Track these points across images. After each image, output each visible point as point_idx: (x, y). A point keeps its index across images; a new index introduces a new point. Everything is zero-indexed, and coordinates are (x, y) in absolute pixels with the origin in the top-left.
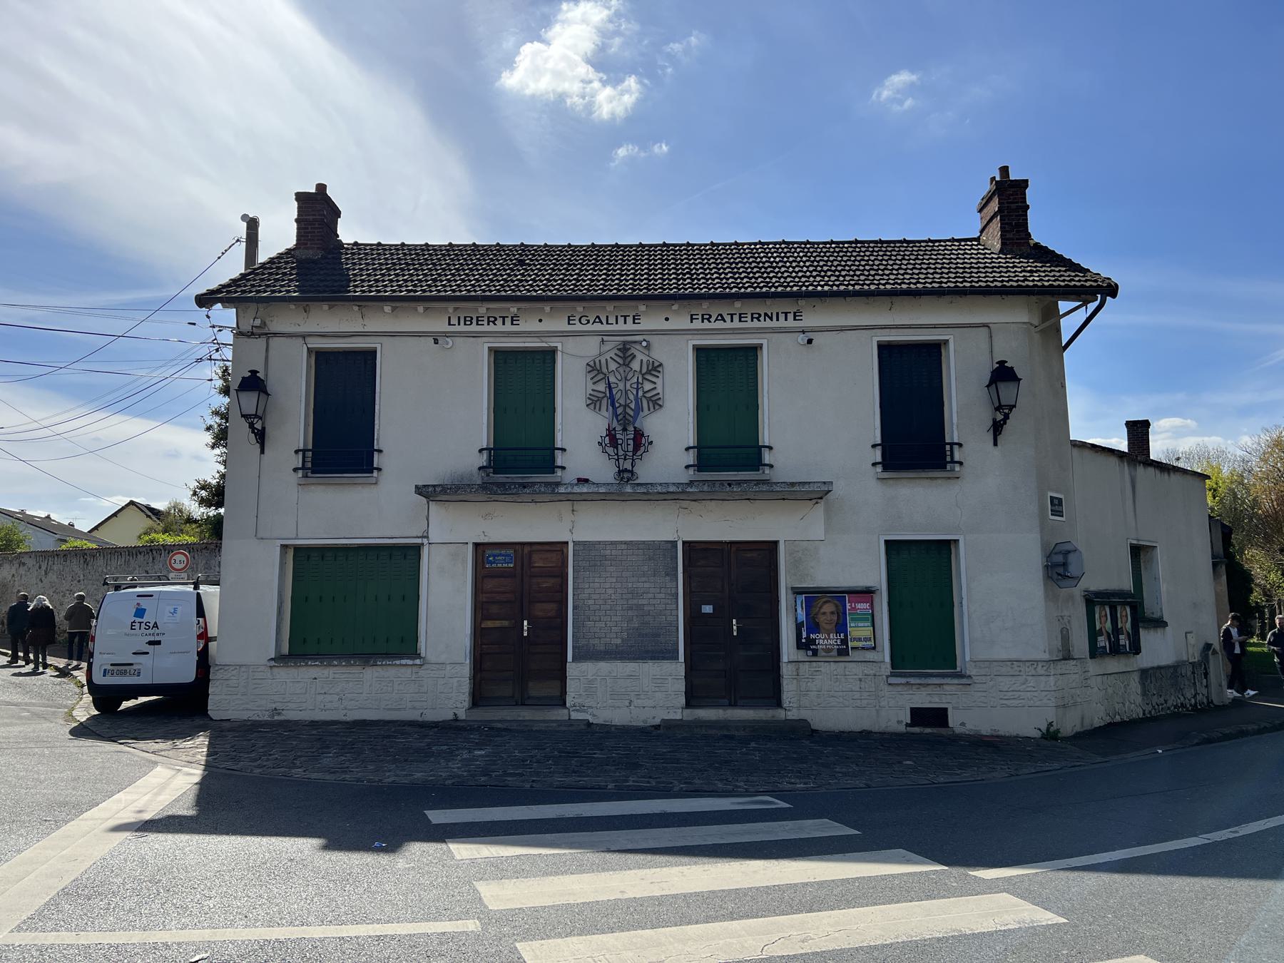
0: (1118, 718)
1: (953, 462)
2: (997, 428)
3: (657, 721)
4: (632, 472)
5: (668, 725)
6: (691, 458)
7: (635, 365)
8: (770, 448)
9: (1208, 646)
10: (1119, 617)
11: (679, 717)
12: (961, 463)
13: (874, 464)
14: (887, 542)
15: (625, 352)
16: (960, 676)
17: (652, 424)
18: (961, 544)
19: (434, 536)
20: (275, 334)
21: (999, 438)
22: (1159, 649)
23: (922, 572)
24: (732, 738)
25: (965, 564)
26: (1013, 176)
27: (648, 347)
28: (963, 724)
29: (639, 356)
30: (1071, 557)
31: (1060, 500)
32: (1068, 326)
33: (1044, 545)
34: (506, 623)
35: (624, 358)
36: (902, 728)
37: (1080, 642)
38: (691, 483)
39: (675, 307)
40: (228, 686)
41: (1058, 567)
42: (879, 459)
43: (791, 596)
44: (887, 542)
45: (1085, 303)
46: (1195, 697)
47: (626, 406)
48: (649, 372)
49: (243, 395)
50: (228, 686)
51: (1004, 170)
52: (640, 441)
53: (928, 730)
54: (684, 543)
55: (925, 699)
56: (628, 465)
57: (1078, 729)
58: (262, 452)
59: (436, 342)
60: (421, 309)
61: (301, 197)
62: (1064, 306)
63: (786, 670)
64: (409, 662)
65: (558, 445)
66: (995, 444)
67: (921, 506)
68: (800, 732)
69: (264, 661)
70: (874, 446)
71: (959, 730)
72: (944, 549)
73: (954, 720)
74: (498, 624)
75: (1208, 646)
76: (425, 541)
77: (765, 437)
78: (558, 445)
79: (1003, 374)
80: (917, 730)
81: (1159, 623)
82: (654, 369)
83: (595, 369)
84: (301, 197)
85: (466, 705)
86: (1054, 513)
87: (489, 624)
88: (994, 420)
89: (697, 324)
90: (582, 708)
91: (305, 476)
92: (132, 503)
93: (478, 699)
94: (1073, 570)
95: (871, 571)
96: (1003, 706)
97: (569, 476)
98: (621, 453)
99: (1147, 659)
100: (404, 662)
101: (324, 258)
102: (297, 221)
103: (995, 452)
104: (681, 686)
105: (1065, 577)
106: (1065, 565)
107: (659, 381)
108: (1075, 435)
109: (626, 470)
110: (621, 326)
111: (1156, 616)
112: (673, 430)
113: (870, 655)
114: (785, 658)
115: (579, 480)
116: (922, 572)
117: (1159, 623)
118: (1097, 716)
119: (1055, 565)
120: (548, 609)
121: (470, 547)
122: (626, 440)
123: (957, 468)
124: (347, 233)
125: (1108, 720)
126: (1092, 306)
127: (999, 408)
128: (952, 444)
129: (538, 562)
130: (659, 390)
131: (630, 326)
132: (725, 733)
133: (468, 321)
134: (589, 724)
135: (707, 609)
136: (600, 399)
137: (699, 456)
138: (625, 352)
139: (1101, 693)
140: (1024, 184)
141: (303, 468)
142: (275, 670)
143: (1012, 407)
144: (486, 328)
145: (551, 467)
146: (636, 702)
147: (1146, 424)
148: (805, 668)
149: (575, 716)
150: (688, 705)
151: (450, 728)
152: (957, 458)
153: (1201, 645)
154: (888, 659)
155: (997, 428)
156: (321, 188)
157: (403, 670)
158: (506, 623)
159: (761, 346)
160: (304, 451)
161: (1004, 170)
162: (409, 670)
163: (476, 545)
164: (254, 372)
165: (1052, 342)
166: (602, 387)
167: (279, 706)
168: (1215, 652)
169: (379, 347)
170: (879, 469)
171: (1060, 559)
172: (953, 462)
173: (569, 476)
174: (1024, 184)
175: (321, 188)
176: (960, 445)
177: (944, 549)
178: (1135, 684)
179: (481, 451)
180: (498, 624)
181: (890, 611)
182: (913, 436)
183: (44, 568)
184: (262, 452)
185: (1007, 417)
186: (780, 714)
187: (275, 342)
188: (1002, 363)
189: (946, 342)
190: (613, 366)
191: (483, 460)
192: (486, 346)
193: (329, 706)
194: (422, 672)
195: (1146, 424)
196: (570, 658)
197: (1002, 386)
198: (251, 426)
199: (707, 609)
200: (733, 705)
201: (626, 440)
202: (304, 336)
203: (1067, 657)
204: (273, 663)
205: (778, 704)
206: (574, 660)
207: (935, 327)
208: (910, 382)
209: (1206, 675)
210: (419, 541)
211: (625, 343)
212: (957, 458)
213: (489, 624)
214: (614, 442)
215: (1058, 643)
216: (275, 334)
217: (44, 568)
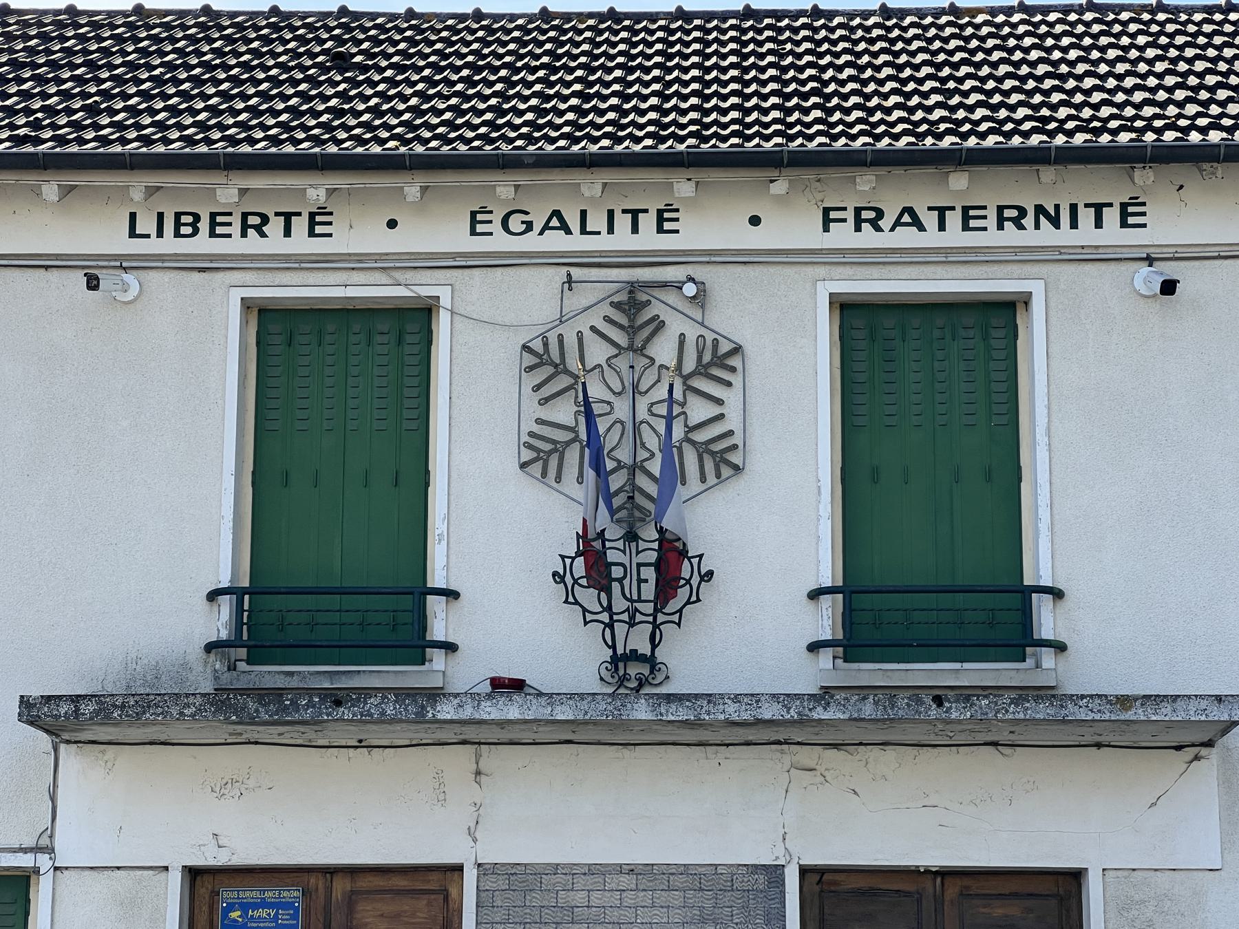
6: (824, 621)
7: (664, 350)
15: (634, 313)
17: (710, 520)
27: (699, 299)
29: (676, 325)
35: (631, 330)
38: (826, 695)
39: (779, 187)
48: (702, 370)
52: (674, 568)
54: (804, 871)
59: (93, 283)
65: (437, 578)
76: (44, 862)
77: (1040, 565)
78: (437, 578)
82: (720, 360)
83: (546, 362)
97: (466, 672)
98: (619, 604)
107: (731, 398)
109: (634, 656)
110: (623, 240)
112: (773, 542)
115: (497, 683)
121: (175, 882)
122: (637, 568)
130: (733, 421)
131: (649, 239)
136: (559, 449)
137: (849, 617)
138: (634, 313)
163: (194, 874)
166: (565, 411)
173: (466, 672)
179: (213, 596)
190: (598, 352)
192: (236, 295)
201: (637, 568)
210: (26, 861)
211: (633, 287)
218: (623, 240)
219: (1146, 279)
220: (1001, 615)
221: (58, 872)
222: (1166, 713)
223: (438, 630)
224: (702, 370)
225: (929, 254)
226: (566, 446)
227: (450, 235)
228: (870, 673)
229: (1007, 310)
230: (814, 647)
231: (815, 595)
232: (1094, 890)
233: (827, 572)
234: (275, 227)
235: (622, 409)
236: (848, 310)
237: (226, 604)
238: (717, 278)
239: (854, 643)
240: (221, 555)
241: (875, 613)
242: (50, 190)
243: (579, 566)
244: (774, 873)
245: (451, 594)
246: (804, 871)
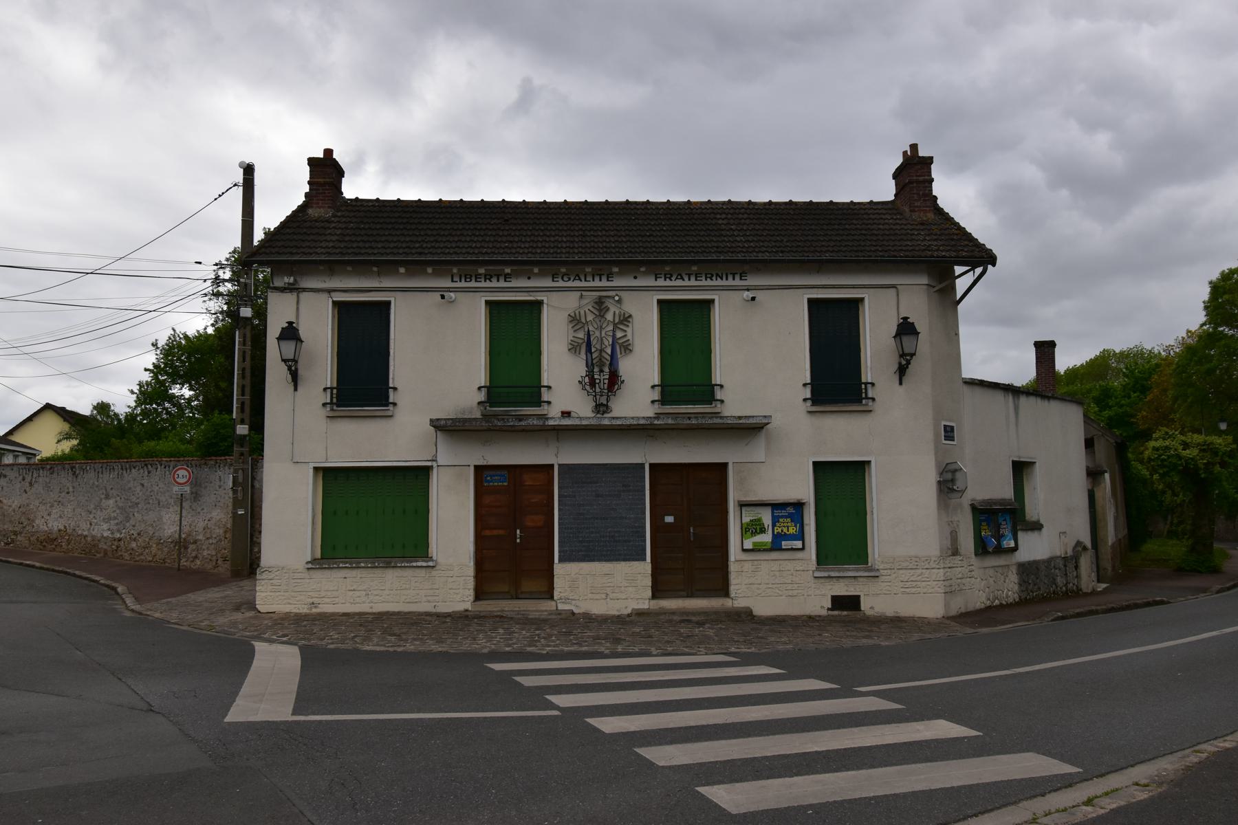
0: (997, 602)
1: (867, 398)
2: (902, 371)
3: (629, 611)
4: (607, 406)
5: (640, 613)
6: (656, 395)
7: (609, 316)
8: (722, 386)
9: (1079, 543)
10: (998, 522)
11: (646, 607)
12: (873, 399)
13: (805, 400)
14: (815, 463)
15: (600, 306)
16: (871, 569)
17: (626, 366)
18: (873, 464)
19: (441, 461)
20: (304, 290)
21: (904, 379)
22: (1032, 549)
23: (842, 481)
24: (689, 621)
25: (875, 480)
26: (922, 153)
27: (619, 301)
28: (872, 608)
29: (613, 309)
30: (958, 475)
31: (952, 428)
32: (961, 284)
33: (938, 464)
34: (501, 532)
35: (600, 310)
36: (824, 613)
37: (967, 542)
38: (658, 416)
39: (643, 269)
40: (272, 585)
41: (948, 484)
42: (809, 396)
43: (738, 509)
44: (815, 463)
45: (973, 269)
46: (1066, 585)
47: (601, 351)
48: (621, 322)
49: (283, 343)
50: (272, 585)
51: (914, 147)
52: (614, 380)
53: (845, 613)
54: (651, 465)
55: (842, 589)
56: (603, 400)
57: (963, 610)
58: (296, 389)
59: (443, 297)
60: (430, 270)
61: (312, 162)
62: (958, 270)
63: (733, 567)
64: (424, 564)
65: (545, 383)
66: (901, 383)
67: (841, 437)
68: (745, 616)
69: (301, 565)
70: (805, 385)
71: (869, 613)
72: (859, 468)
73: (865, 605)
74: (496, 532)
75: (1079, 543)
76: (435, 464)
77: (717, 378)
78: (545, 383)
79: (906, 329)
80: (836, 613)
81: (1036, 527)
82: (626, 319)
83: (575, 321)
84: (312, 162)
85: (472, 598)
86: (947, 438)
87: (487, 533)
88: (900, 364)
89: (661, 282)
90: (566, 600)
91: (332, 410)
92: (48, 407)
93: (479, 595)
94: (959, 485)
95: (802, 488)
96: (904, 593)
97: (554, 412)
98: (598, 390)
99: (1024, 555)
100: (419, 564)
101: (334, 216)
102: (309, 183)
103: (901, 389)
104: (648, 582)
105: (953, 490)
106: (953, 481)
107: (629, 330)
108: (967, 374)
109: (602, 405)
110: (597, 283)
111: (1034, 519)
112: (642, 369)
113: (800, 555)
114: (732, 558)
115: (563, 413)
116: (842, 481)
117: (1036, 527)
118: (979, 605)
119: (946, 481)
120: (533, 520)
121: (472, 469)
122: (604, 379)
123: (870, 403)
124: (351, 189)
125: (988, 603)
126: (979, 270)
127: (902, 355)
128: (866, 384)
129: (528, 480)
130: (629, 337)
131: (604, 283)
132: (686, 618)
133: (468, 277)
134: (573, 614)
135: (669, 519)
136: (580, 345)
137: (662, 393)
138: (600, 306)
139: (987, 583)
140: (930, 160)
141: (331, 403)
142: (312, 572)
143: (912, 355)
144: (483, 284)
145: (538, 402)
146: (611, 596)
147: (1052, 344)
148: (747, 566)
149: (561, 607)
150: (654, 597)
151: (461, 619)
152: (870, 395)
153: (1073, 544)
154: (814, 557)
155: (902, 371)
156: (329, 152)
157: (418, 571)
158: (501, 532)
159: (713, 301)
160: (332, 389)
161: (914, 147)
162: (423, 571)
163: (476, 467)
164: (290, 323)
165: (947, 299)
166: (581, 335)
167: (316, 600)
168: (1085, 548)
169: (392, 300)
170: (809, 403)
171: (949, 476)
172: (867, 398)
173: (554, 412)
174: (930, 160)
175: (329, 152)
176: (873, 384)
177: (859, 468)
178: (1013, 577)
179: (480, 388)
180: (496, 532)
181: (817, 531)
182: (836, 380)
183: (28, 479)
184: (296, 389)
185: (908, 363)
186: (728, 603)
187: (303, 296)
188: (905, 319)
189: (862, 300)
190: (590, 317)
191: (482, 396)
192: (483, 300)
193: (358, 600)
194: (434, 573)
195: (1052, 344)
196: (556, 560)
197: (905, 339)
198: (289, 368)
199: (669, 519)
200: (691, 595)
201: (604, 379)
202: (329, 291)
203: (955, 552)
204: (310, 566)
205: (726, 594)
206: (560, 561)
207: (854, 287)
208: (834, 335)
209: (1077, 567)
210: (429, 464)
211: (600, 297)
212: (870, 395)
213: (487, 533)
214: (593, 383)
215: (948, 543)
216: (304, 290)
217: (28, 479)
218: (597, 283)
219: (437, 296)
220: (707, 392)
221: (744, 509)
222: (751, 421)
223: (545, 397)
224: (621, 322)
225: (685, 289)
226: (584, 346)
227: (547, 282)
228: (669, 409)
229: (538, 304)
230: (653, 402)
231: (653, 387)
232: (730, 467)
233: (657, 381)
234: (730, 277)
235: (597, 333)
236: (810, 301)
237: (484, 391)
238: (624, 294)
239: (664, 400)
240: (482, 378)
241: (668, 392)
242: (430, 270)
243: (587, 380)
244: (642, 465)
245: (549, 387)
246: (651, 465)
